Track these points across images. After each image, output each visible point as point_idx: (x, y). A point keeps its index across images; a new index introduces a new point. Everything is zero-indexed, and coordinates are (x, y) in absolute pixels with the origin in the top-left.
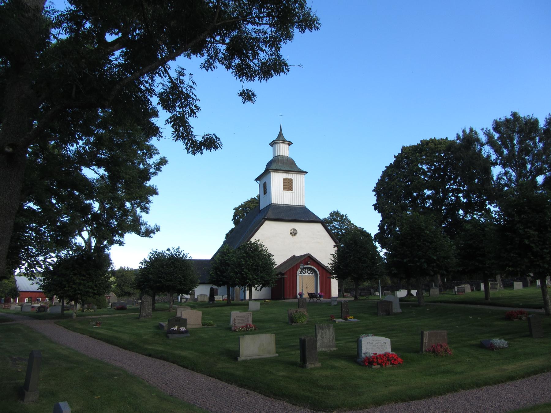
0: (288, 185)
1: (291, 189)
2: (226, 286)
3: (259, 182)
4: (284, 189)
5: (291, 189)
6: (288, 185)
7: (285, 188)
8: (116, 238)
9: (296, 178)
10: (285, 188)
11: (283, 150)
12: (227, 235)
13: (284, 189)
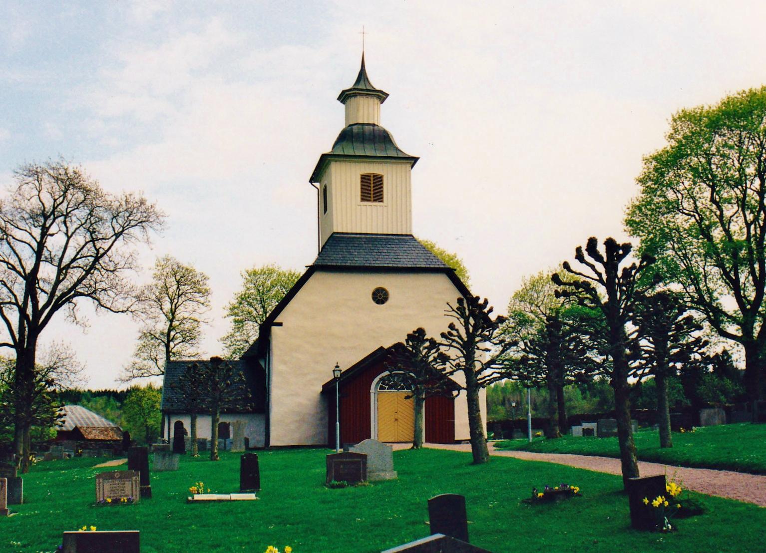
0: (372, 190)
1: (379, 197)
2: (469, 438)
3: (317, 185)
4: (363, 200)
5: (379, 197)
6: (372, 190)
7: (365, 197)
8: (668, 293)
9: (389, 174)
10: (365, 197)
11: (369, 113)
12: (607, 239)
13: (363, 200)
